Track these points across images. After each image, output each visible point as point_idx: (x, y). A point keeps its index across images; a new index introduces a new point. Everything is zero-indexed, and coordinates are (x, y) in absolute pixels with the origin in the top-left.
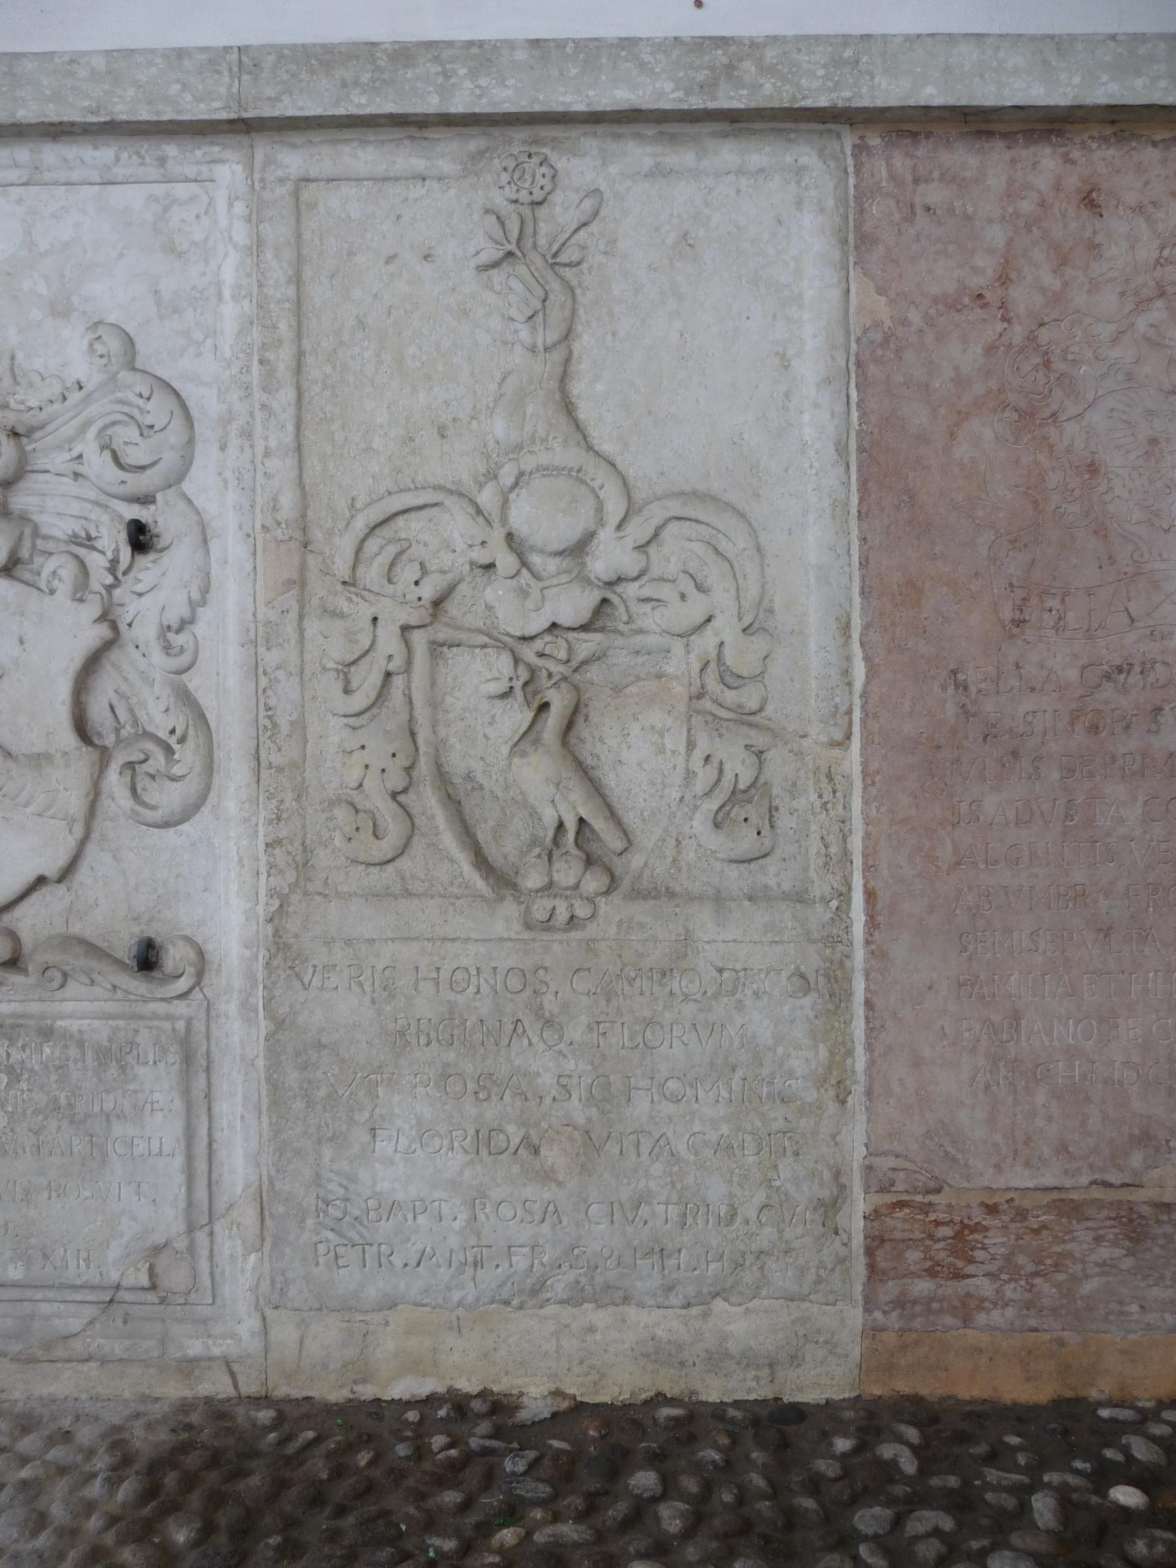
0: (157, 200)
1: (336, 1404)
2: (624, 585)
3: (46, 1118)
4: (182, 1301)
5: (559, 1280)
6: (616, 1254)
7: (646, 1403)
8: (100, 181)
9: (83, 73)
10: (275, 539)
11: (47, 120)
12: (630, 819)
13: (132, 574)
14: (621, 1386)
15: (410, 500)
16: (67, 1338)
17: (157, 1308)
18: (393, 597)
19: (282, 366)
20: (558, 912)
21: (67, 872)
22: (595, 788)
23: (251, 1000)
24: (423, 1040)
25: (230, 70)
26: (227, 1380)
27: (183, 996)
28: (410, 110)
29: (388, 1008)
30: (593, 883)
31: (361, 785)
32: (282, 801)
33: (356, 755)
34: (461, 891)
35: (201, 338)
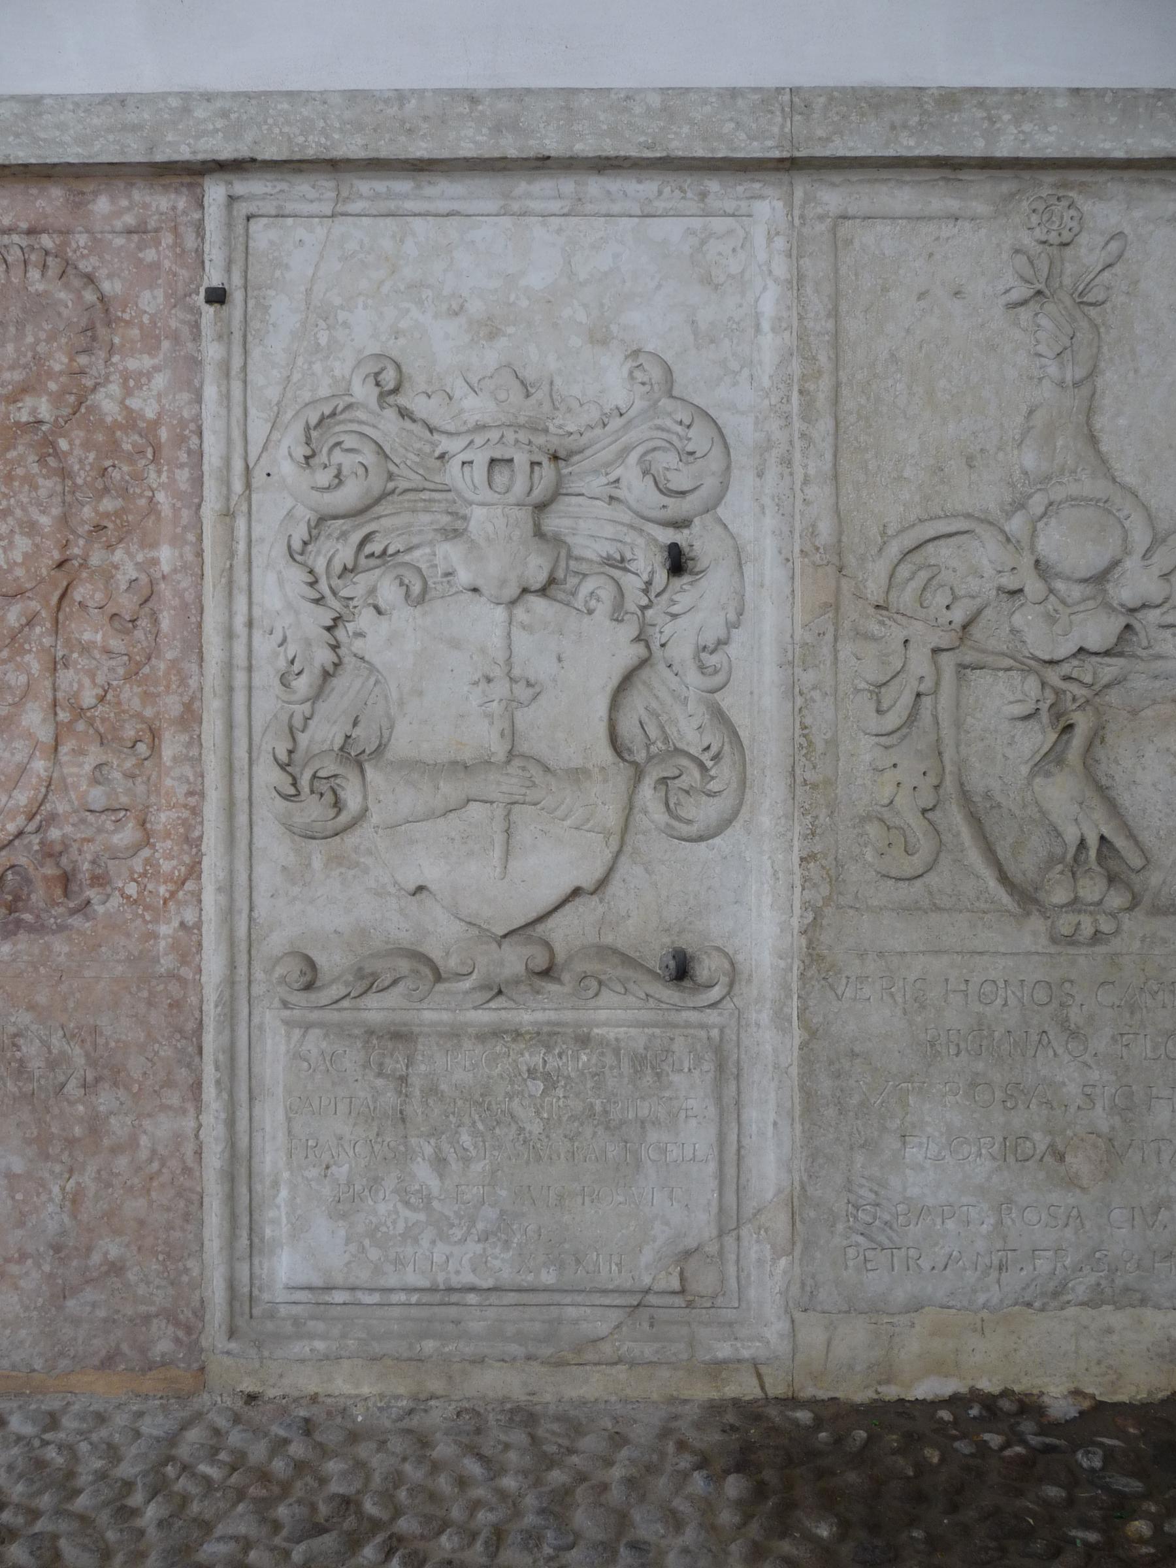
0: (694, 233)
1: (861, 1405)
2: (1145, 611)
3: (582, 1124)
4: (709, 1305)
5: (1080, 1283)
6: (1136, 1257)
7: (932, 1402)
8: (639, 213)
9: (638, 110)
10: (814, 563)
11: (604, 154)
12: (1146, 837)
13: (666, 596)
14: (1137, 1386)
15: (943, 527)
16: (594, 1341)
17: (682, 1311)
18: (925, 621)
19: (821, 397)
20: (1083, 927)
21: (602, 883)
22: (1113, 807)
23: (786, 1010)
24: (953, 1051)
25: (783, 110)
26: (754, 1382)
27: (713, 1005)
28: (958, 153)
29: (919, 1019)
30: (1117, 900)
31: (891, 802)
32: (817, 817)
33: (888, 775)
34: (987, 906)
35: (737, 369)
